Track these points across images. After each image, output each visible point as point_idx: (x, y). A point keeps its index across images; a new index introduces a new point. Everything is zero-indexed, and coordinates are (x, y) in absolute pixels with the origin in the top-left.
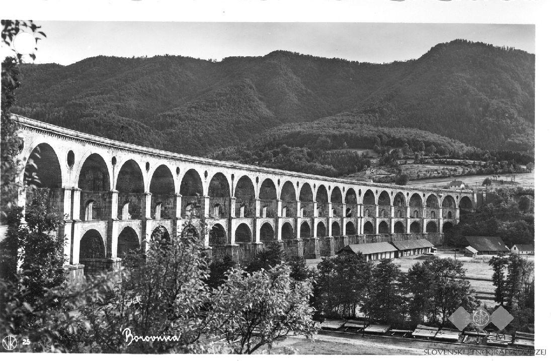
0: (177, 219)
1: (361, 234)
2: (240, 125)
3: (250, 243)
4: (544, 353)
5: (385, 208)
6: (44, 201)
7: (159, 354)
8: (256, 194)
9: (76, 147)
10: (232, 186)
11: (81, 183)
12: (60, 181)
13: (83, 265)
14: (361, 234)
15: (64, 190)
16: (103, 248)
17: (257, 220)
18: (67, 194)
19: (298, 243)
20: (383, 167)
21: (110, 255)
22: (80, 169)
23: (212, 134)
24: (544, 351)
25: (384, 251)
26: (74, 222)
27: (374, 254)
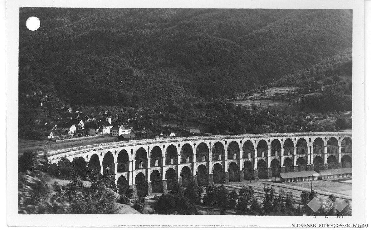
0: (178, 165)
1: (310, 163)
2: (324, 41)
3: (222, 172)
4: (367, 226)
5: (336, 147)
6: (134, 119)
7: (159, 214)
8: (225, 149)
9: (133, 147)
10: (210, 148)
11: (136, 159)
12: (128, 159)
13: (151, 182)
14: (310, 163)
15: (129, 162)
16: (144, 178)
17: (226, 161)
18: (131, 163)
19: (255, 171)
20: (43, 209)
21: (147, 180)
22: (135, 154)
23: (298, 51)
24: (367, 225)
25: (346, 173)
26: (133, 171)
27: (298, 178)
